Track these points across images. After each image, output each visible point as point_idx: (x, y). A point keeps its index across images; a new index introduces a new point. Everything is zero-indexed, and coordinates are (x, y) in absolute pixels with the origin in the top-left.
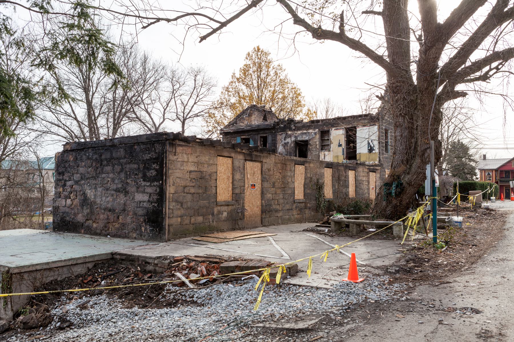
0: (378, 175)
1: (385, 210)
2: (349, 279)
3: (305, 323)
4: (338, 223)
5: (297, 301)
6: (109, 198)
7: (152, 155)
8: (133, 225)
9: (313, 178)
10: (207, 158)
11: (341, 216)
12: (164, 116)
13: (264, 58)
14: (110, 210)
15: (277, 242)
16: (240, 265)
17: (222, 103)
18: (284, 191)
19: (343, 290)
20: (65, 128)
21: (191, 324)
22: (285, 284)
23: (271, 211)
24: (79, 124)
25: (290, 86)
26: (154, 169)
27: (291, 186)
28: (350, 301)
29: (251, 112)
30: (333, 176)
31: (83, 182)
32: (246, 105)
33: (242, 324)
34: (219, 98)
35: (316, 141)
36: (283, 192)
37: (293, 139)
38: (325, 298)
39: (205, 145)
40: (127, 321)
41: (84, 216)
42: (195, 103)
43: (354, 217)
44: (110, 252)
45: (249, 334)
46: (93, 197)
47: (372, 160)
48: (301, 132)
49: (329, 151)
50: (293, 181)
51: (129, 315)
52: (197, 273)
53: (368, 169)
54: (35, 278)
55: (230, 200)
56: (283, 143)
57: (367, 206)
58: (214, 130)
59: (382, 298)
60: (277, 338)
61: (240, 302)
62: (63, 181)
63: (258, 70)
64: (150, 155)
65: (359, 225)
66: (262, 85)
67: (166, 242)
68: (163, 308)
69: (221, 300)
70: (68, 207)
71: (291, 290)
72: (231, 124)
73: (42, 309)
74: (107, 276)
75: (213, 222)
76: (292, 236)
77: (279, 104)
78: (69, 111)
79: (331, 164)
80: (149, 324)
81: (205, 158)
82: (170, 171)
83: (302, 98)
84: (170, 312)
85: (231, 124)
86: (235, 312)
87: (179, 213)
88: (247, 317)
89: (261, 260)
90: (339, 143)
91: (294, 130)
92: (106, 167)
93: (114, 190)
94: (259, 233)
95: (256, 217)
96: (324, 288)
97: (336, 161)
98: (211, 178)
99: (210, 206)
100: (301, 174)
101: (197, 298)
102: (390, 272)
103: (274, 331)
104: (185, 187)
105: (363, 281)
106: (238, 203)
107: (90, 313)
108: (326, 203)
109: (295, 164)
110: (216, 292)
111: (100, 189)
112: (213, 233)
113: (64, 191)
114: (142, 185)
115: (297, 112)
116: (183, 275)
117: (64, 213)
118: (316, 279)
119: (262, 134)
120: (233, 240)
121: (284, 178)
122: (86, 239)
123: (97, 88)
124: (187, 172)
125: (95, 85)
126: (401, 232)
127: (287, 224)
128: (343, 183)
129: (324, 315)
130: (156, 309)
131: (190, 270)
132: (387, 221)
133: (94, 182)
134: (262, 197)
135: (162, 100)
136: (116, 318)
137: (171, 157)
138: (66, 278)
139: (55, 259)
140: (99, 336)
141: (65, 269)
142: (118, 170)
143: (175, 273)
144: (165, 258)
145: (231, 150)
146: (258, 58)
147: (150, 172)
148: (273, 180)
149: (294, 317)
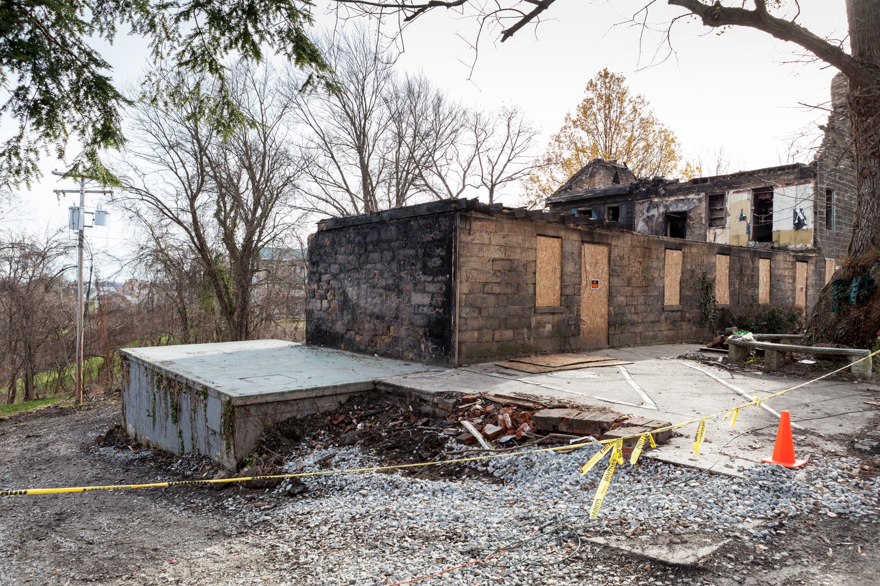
0: (812, 267)
1: (833, 328)
2: (773, 459)
3: (690, 552)
4: (744, 348)
5: (671, 496)
6: (376, 299)
7: (435, 235)
8: (408, 341)
9: (697, 271)
11: (749, 336)
12: (464, 181)
13: (615, 87)
14: (378, 318)
15: (633, 376)
16: (568, 417)
17: (549, 160)
18: (647, 292)
19: (765, 482)
20: (335, 203)
21: (477, 517)
22: (648, 458)
23: (624, 323)
24: (352, 198)
25: (657, 128)
26: (439, 255)
27: (659, 284)
28: (783, 510)
29: (595, 170)
30: (731, 269)
31: (342, 275)
32: (585, 161)
33: (566, 532)
34: (544, 152)
35: (700, 212)
36: (645, 294)
38: (728, 496)
39: (517, 218)
40: (382, 495)
41: (344, 325)
42: (509, 161)
43: (770, 337)
44: (371, 380)
45: (577, 558)
46: (355, 298)
47: (801, 241)
48: (676, 198)
49: (724, 228)
50: (662, 276)
51: (386, 485)
52: (496, 424)
53: (793, 256)
54: (266, 414)
55: (556, 305)
56: (645, 216)
57: (793, 318)
58: (538, 201)
59: (853, 509)
60: (633, 577)
61: (564, 486)
62: (318, 275)
63: (605, 107)
64: (432, 235)
65: (782, 352)
66: (613, 130)
67: (456, 368)
68: (439, 480)
69: (533, 477)
70: (325, 312)
71: (660, 472)
72: (563, 190)
73: (273, 459)
74: (366, 417)
75: (529, 339)
76: (659, 367)
77: (639, 157)
78: (339, 180)
79: (727, 248)
80: (413, 507)
81: (517, 239)
82: (462, 260)
83: (677, 146)
84: (447, 489)
85: (563, 190)
86: (556, 503)
87: (476, 324)
88: (575, 519)
89: (604, 409)
90: (742, 215)
91: (664, 195)
92: (372, 254)
93: (382, 288)
94: (602, 359)
95: (599, 332)
96: (724, 474)
97: (735, 243)
98: (526, 270)
99: (524, 313)
100: (677, 264)
101: (494, 467)
102: (860, 449)
103: (627, 558)
104: (485, 284)
105: (805, 465)
106: (570, 309)
107: (331, 475)
108: (717, 312)
109: (666, 249)
110: (525, 460)
111: (364, 286)
112: (529, 356)
113: (319, 289)
114: (421, 280)
115: (669, 169)
116: (475, 426)
117: (319, 319)
118: (707, 453)
119: (610, 203)
120: (560, 370)
121: (647, 270)
122: (346, 357)
123: (374, 146)
124: (489, 261)
125: (371, 143)
126: (868, 369)
127: (651, 344)
128: (748, 280)
129: (728, 537)
130: (427, 480)
131: (485, 417)
132: (838, 347)
133: (357, 276)
134: (609, 301)
135: (461, 158)
136: (366, 488)
137: (464, 237)
138: (308, 415)
139: (293, 387)
140: (337, 517)
141: (307, 403)
142: (389, 258)
143: (462, 422)
144: (450, 395)
145: (558, 226)
146: (606, 87)
147: (433, 260)
148: (628, 274)
149: (667, 532)
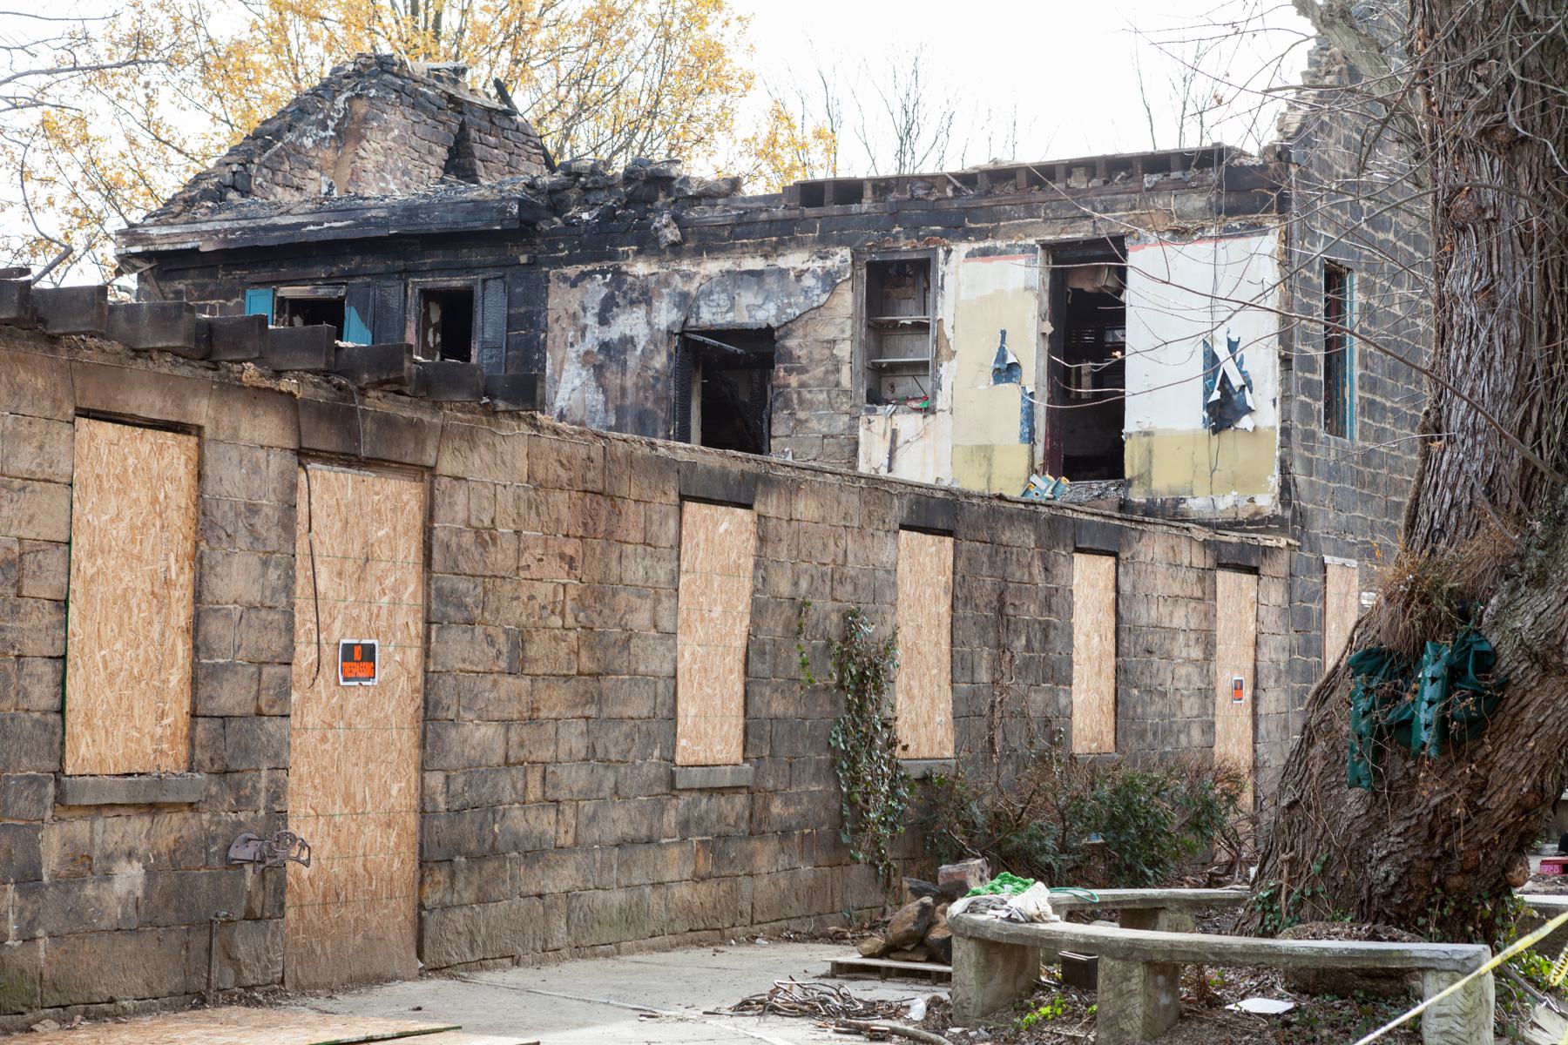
37: (666, 315)
145: (185, 371)
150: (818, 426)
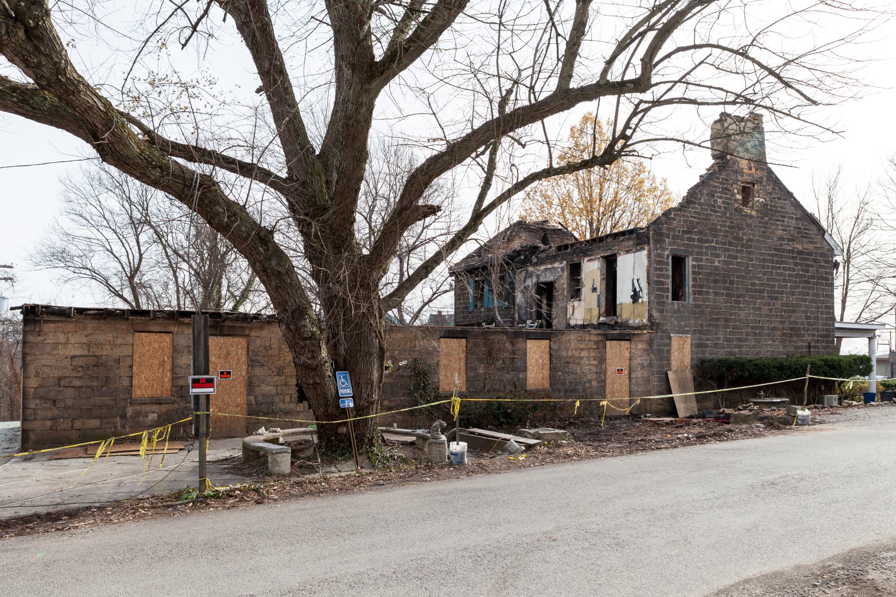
10: (110, 337)
37: (535, 280)
99: (116, 404)
104: (60, 379)
145: (167, 322)
150: (561, 305)
